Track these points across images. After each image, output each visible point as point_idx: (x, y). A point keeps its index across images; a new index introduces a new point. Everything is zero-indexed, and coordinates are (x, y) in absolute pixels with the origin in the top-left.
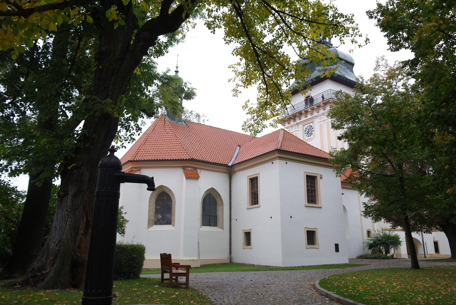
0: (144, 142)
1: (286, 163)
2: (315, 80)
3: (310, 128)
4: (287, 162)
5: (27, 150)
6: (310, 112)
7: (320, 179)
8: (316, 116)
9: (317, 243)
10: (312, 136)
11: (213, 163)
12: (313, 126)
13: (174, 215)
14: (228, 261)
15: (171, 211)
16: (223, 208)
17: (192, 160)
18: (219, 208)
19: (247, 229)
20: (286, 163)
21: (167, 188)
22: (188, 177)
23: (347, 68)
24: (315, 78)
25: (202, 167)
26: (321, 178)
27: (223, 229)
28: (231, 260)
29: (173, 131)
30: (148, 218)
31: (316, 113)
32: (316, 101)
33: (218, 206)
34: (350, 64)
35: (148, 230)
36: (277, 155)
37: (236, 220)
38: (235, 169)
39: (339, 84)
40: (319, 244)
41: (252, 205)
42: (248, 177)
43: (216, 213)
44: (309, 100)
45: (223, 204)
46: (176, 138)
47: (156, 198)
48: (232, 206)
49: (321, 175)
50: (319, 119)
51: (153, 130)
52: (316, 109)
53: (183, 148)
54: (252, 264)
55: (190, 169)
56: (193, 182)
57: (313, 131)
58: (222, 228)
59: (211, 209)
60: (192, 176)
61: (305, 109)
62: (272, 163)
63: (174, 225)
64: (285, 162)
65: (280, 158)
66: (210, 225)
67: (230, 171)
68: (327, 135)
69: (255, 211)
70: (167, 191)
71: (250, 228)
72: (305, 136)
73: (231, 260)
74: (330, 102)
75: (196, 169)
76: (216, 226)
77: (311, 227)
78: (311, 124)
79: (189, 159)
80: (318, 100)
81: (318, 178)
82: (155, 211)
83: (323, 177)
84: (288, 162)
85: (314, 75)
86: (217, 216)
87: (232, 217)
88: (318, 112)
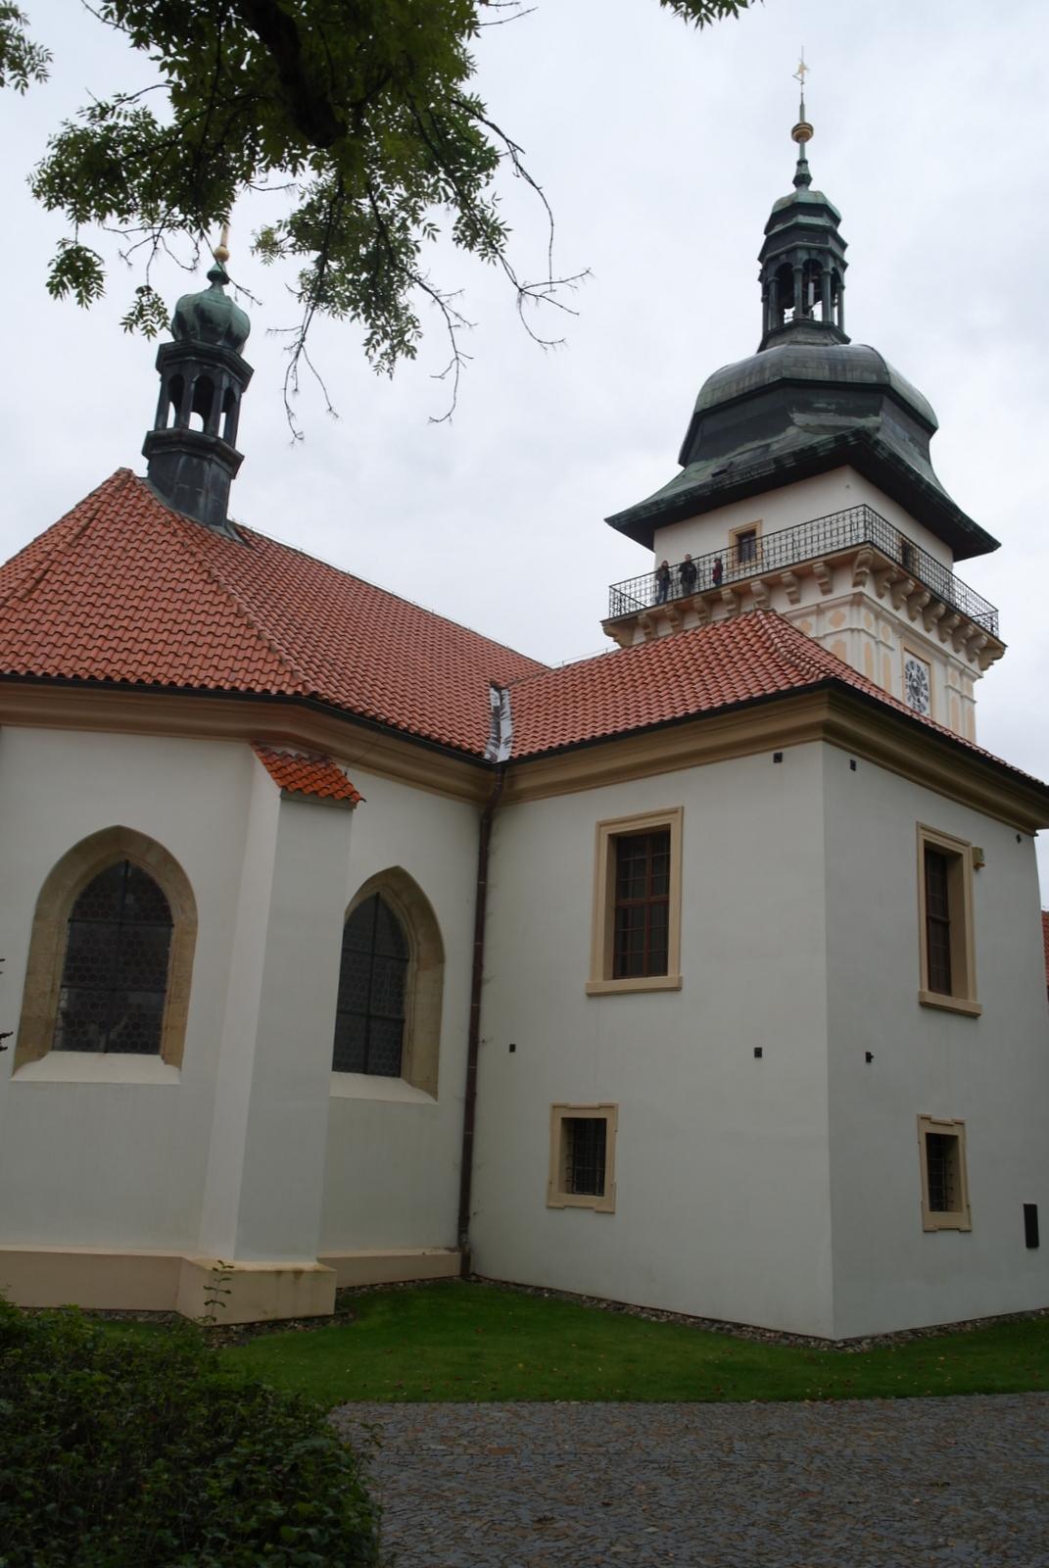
0: (28, 585)
1: (853, 766)
2: (790, 463)
4: (856, 758)
6: (760, 595)
7: (973, 872)
9: (964, 1201)
11: (417, 734)
13: (184, 999)
14: (452, 1268)
15: (164, 974)
16: (439, 981)
17: (314, 703)
18: (418, 982)
19: (584, 1099)
20: (853, 766)
21: (150, 844)
22: (295, 792)
23: (910, 440)
24: (794, 454)
25: (357, 752)
26: (978, 866)
27: (434, 1093)
28: (466, 1260)
29: (193, 554)
30: (24, 1008)
31: (819, 593)
33: (412, 966)
34: (924, 425)
35: (16, 1078)
36: (823, 715)
37: (512, 1048)
38: (524, 784)
40: (972, 1209)
41: (615, 977)
42: (601, 825)
43: (401, 1003)
45: (439, 958)
46: (214, 587)
47: (74, 898)
48: (487, 974)
49: (978, 853)
50: (831, 622)
51: (77, 537)
52: (789, 585)
53: (259, 638)
54: (504, 1279)
55: (293, 752)
56: (318, 826)
58: (431, 1087)
59: (383, 974)
60: (316, 789)
61: (658, 604)
62: (778, 758)
63: (174, 1059)
64: (849, 757)
65: (833, 734)
66: (365, 1068)
67: (489, 792)
69: (639, 1011)
70: (150, 865)
71: (959, 1118)
73: (466, 1260)
74: (860, 557)
75: (325, 755)
76: (399, 1076)
77: (943, 1113)
79: (297, 693)
81: (967, 863)
82: (67, 968)
83: (987, 859)
84: (860, 763)
85: (783, 444)
86: (402, 1022)
87: (484, 1033)
88: (795, 596)
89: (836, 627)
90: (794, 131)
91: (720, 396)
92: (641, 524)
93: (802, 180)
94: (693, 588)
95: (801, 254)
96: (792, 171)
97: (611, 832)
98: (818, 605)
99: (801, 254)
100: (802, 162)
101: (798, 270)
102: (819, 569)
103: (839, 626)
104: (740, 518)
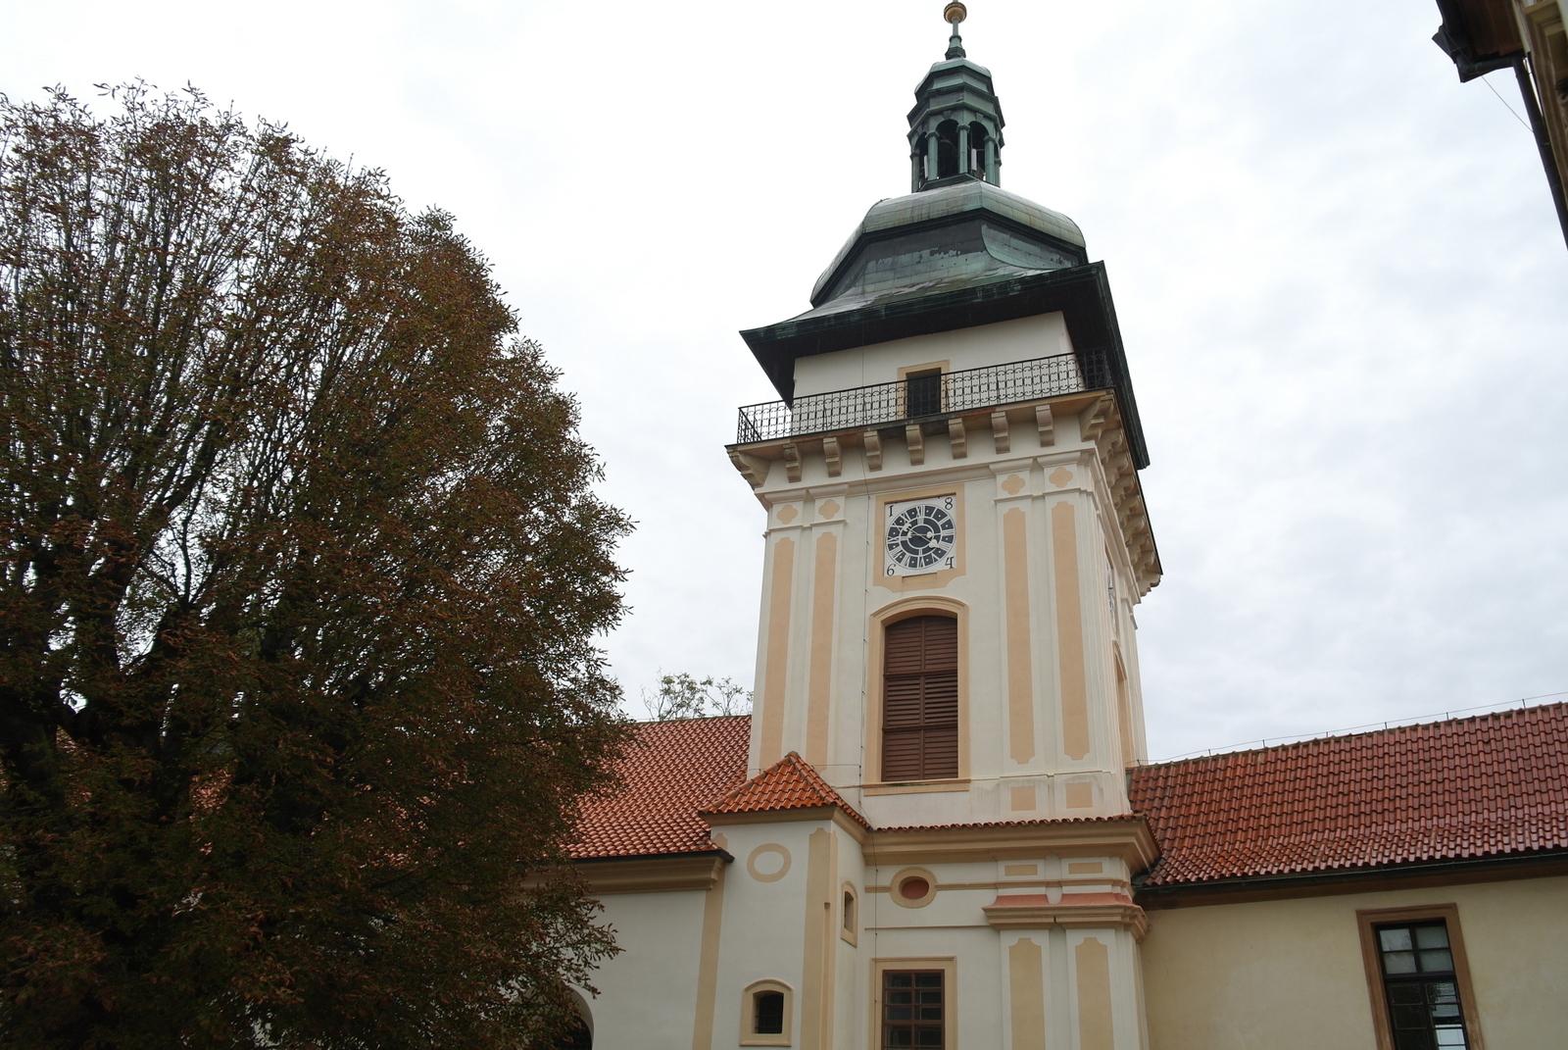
3: (926, 521)
5: (159, 367)
8: (986, 466)
10: (940, 565)
12: (951, 514)
32: (892, 395)
39: (1033, 317)
44: (924, 390)
57: (950, 539)
68: (806, 723)
72: (890, 561)
78: (939, 504)
80: (958, 396)
88: (918, 456)
89: (784, 523)
90: (947, 9)
91: (882, 225)
92: (779, 350)
93: (955, 51)
94: (116, 659)
95: (955, 119)
96: (946, 46)
97: (1374, 921)
98: (1035, 459)
99: (955, 119)
100: (956, 37)
101: (964, 128)
102: (830, 445)
103: (1017, 492)
104: (918, 357)
